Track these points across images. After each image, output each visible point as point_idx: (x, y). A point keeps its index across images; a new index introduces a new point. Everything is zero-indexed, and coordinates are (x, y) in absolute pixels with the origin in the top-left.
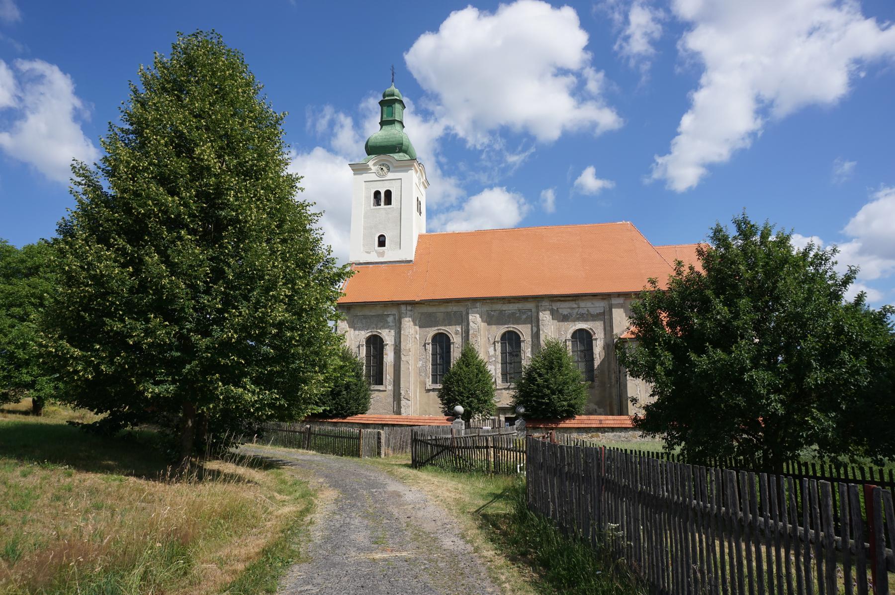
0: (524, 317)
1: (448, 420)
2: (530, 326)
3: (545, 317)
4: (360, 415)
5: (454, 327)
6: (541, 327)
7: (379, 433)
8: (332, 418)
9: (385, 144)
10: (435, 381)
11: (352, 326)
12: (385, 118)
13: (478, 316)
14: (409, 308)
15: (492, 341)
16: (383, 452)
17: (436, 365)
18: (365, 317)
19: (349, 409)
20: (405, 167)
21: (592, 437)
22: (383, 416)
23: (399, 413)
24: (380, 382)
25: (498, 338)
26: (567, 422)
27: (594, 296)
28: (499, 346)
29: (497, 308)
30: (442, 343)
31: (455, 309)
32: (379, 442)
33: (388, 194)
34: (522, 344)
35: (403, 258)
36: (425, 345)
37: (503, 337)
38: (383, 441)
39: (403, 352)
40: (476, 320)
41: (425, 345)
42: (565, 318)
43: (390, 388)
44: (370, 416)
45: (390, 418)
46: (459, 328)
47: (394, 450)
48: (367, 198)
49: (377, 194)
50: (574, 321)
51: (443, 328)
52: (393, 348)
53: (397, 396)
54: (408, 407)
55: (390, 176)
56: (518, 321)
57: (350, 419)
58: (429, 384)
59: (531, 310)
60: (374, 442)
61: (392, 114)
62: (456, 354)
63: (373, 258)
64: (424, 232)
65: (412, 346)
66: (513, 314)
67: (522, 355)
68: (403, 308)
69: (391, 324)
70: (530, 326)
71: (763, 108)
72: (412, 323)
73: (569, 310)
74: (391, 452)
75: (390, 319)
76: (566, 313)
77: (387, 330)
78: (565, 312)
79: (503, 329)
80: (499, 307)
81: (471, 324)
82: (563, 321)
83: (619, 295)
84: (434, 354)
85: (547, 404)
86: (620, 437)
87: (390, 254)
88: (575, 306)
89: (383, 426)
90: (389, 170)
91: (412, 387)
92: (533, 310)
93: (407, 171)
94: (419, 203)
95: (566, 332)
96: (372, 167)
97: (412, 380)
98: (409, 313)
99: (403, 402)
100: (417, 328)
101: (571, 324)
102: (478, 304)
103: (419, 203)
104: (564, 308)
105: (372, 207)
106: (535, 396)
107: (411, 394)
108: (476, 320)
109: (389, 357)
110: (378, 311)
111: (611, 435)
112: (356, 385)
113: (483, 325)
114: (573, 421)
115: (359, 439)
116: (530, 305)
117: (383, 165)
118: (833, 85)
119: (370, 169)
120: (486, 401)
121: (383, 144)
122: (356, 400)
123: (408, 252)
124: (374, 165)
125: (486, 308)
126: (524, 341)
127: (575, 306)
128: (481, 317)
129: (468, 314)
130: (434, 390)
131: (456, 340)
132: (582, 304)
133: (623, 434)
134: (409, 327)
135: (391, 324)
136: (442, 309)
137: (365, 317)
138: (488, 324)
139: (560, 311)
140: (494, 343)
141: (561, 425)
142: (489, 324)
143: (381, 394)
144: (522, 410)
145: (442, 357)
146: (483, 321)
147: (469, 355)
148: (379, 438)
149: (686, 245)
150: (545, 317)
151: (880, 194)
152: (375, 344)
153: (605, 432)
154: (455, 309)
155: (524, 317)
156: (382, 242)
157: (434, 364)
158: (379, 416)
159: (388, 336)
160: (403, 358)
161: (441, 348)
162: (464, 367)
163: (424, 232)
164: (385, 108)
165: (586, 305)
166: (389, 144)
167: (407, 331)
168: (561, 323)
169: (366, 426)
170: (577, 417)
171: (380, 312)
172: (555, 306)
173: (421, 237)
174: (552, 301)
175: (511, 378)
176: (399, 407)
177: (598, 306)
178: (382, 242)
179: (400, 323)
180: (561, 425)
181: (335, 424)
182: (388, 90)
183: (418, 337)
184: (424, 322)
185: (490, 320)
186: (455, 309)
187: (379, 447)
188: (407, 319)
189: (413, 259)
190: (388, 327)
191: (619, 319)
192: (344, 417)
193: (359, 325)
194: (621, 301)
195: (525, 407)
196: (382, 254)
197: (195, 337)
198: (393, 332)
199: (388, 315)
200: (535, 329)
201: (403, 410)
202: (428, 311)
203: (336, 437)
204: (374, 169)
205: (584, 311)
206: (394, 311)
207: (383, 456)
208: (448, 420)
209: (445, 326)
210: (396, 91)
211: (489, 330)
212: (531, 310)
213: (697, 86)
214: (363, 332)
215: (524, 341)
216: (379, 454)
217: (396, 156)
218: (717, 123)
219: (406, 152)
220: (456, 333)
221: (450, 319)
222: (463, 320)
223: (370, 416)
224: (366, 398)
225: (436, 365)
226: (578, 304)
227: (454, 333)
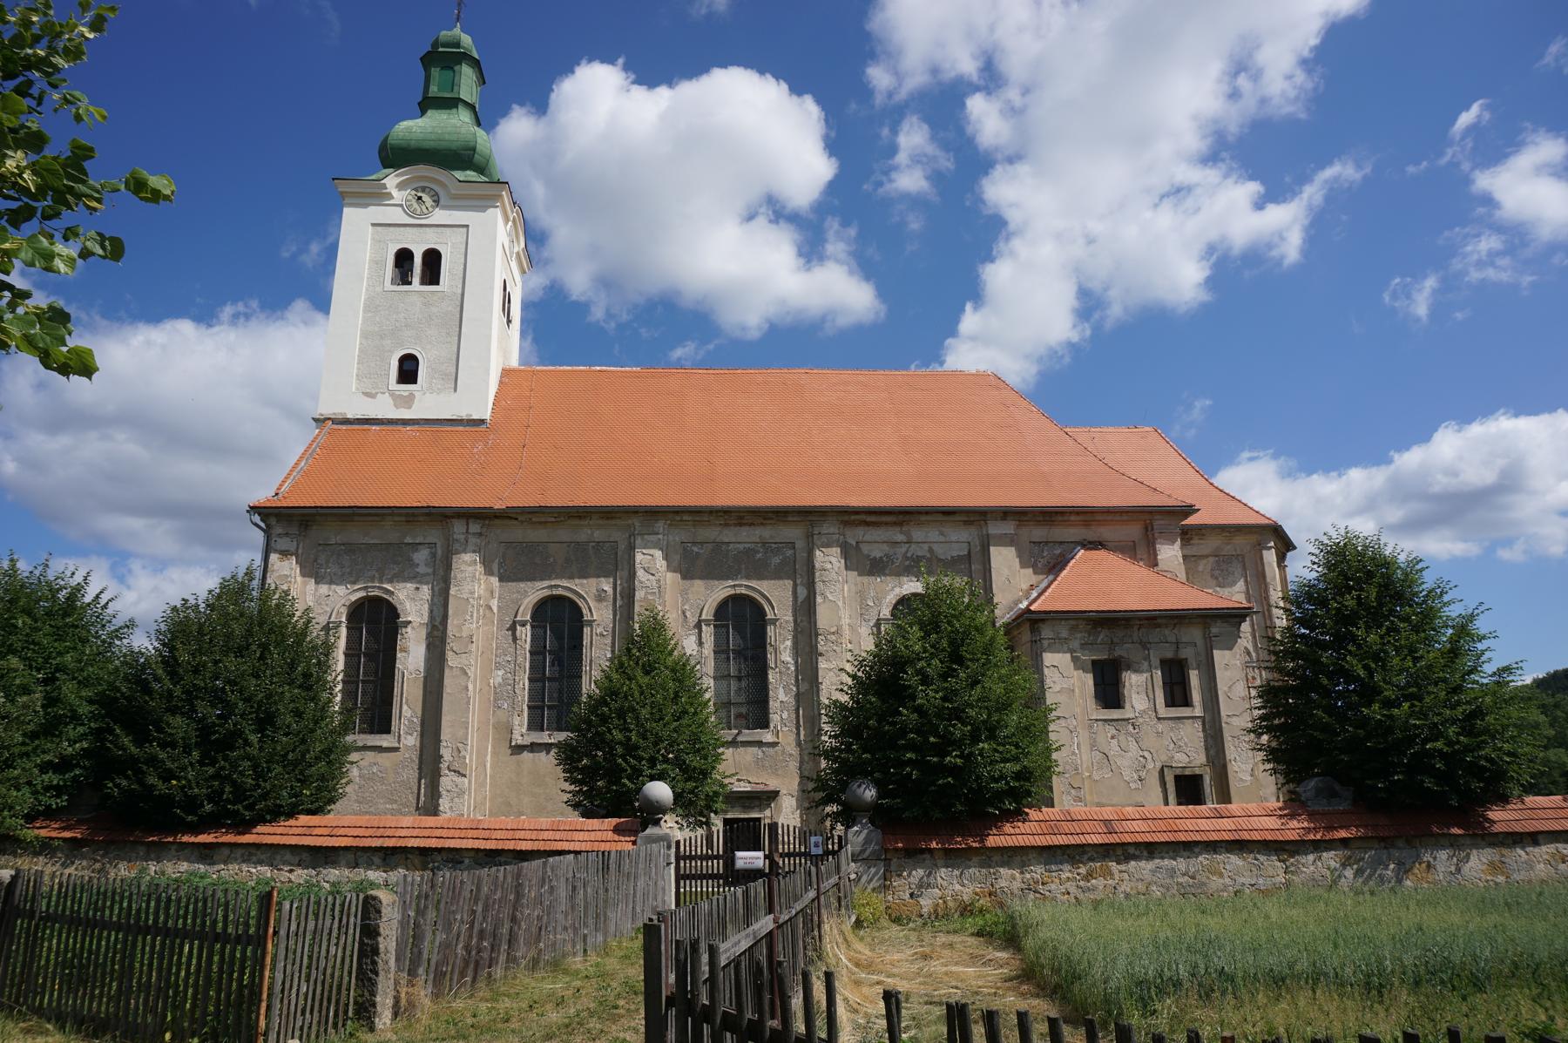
0: (776, 560)
1: (617, 830)
2: (789, 583)
3: (829, 561)
4: (304, 819)
5: (593, 581)
6: (819, 586)
7: (370, 907)
8: (196, 829)
9: (432, 144)
10: (535, 724)
11: (312, 570)
12: (434, 90)
13: (658, 554)
14: (475, 527)
15: (692, 620)
16: (384, 1002)
17: (542, 679)
18: (350, 548)
19: (265, 796)
20: (481, 202)
21: (1089, 876)
22: (390, 821)
23: (433, 810)
24: (380, 721)
25: (708, 614)
26: (1008, 828)
27: (948, 513)
28: (708, 632)
29: (714, 535)
30: (558, 624)
31: (598, 535)
32: (369, 952)
33: (433, 259)
34: (770, 630)
35: (463, 413)
36: (513, 628)
37: (722, 610)
38: (388, 941)
39: (452, 644)
40: (652, 566)
41: (513, 628)
42: (876, 567)
43: (411, 741)
44: (342, 822)
45: (409, 829)
46: (607, 586)
47: (438, 978)
48: (378, 263)
49: (403, 258)
50: (898, 574)
51: (565, 583)
52: (424, 633)
53: (430, 764)
54: (461, 793)
55: (440, 216)
56: (760, 572)
57: (265, 834)
58: (521, 732)
59: (792, 545)
60: (340, 951)
61: (453, 85)
62: (598, 653)
63: (383, 408)
64: (514, 362)
65: (478, 628)
66: (749, 553)
67: (770, 657)
68: (458, 527)
69: (422, 569)
70: (789, 583)
71: (1089, 304)
72: (480, 568)
73: (885, 547)
74: (423, 994)
75: (421, 556)
76: (877, 554)
77: (410, 586)
78: (877, 553)
79: (721, 590)
80: (710, 533)
81: (640, 573)
82: (871, 573)
83: (1006, 513)
84: (537, 652)
85: (953, 770)
86: (1172, 873)
87: (427, 401)
88: (900, 538)
89: (390, 856)
90: (437, 202)
91: (473, 739)
92: (800, 544)
93: (483, 209)
94: (507, 299)
95: (878, 601)
96: (395, 193)
97: (474, 719)
98: (472, 540)
99: (447, 781)
100: (494, 580)
101: (890, 581)
102: (660, 525)
103: (507, 299)
104: (875, 542)
105: (388, 285)
106: (912, 746)
107: (470, 758)
108: (652, 566)
109: (412, 657)
110: (389, 533)
111: (1144, 867)
112: (298, 714)
113: (671, 578)
114: (1023, 827)
115: (260, 941)
116: (792, 532)
117: (423, 189)
118: (1185, 279)
119: (390, 196)
120: (705, 774)
121: (426, 145)
122: (296, 763)
123: (477, 397)
124: (401, 186)
125: (677, 536)
126: (774, 622)
127: (900, 538)
128: (666, 558)
129: (631, 549)
130: (533, 747)
131: (600, 615)
132: (918, 534)
133: (1181, 864)
134: (474, 581)
135: (422, 569)
136: (564, 534)
137: (350, 548)
138: (684, 577)
139: (865, 549)
140: (698, 626)
141: (993, 841)
142: (687, 575)
143: (385, 759)
144: (869, 794)
145: (558, 661)
146: (670, 568)
147: (643, 647)
148: (370, 932)
149: (1111, 429)
150: (829, 561)
151: (1246, 455)
152: (376, 623)
153: (1128, 858)
154: (599, 534)
155: (776, 560)
156: (408, 370)
157: (537, 677)
158: (375, 821)
159: (412, 602)
160: (452, 660)
161: (558, 635)
162: (639, 672)
163: (514, 362)
164: (435, 72)
165: (926, 537)
166: (444, 145)
167: (467, 587)
168: (866, 579)
169: (321, 856)
170: (1033, 814)
171: (393, 537)
172: (854, 535)
173: (506, 373)
174: (846, 523)
175: (739, 716)
176: (434, 793)
177: (957, 539)
178: (408, 370)
179: (448, 567)
180: (993, 841)
181: (206, 853)
182: (445, 34)
183: (494, 604)
184: (512, 566)
185: (689, 566)
186: (598, 535)
187: (367, 977)
188: (467, 557)
189: (487, 416)
190: (415, 578)
191: (1006, 572)
192: (245, 826)
193: (333, 569)
194: (1008, 528)
195: (878, 784)
196: (408, 401)
197: (25, 698)
198: (426, 590)
199: (415, 546)
200: (802, 592)
201: (444, 804)
202: (523, 536)
203: (134, 928)
204: (398, 196)
205: (922, 551)
206: (433, 535)
207: (384, 1019)
208: (617, 830)
209: (571, 577)
210: (466, 40)
211: (684, 593)
212: (792, 545)
213: (990, 258)
214: (341, 590)
215: (774, 622)
216: (365, 1012)
217: (459, 175)
218: (1020, 315)
219: (481, 170)
220: (600, 597)
221: (584, 562)
222: (619, 566)
223: (342, 822)
224: (334, 757)
225: (542, 679)
226: (908, 534)
227: (594, 596)
